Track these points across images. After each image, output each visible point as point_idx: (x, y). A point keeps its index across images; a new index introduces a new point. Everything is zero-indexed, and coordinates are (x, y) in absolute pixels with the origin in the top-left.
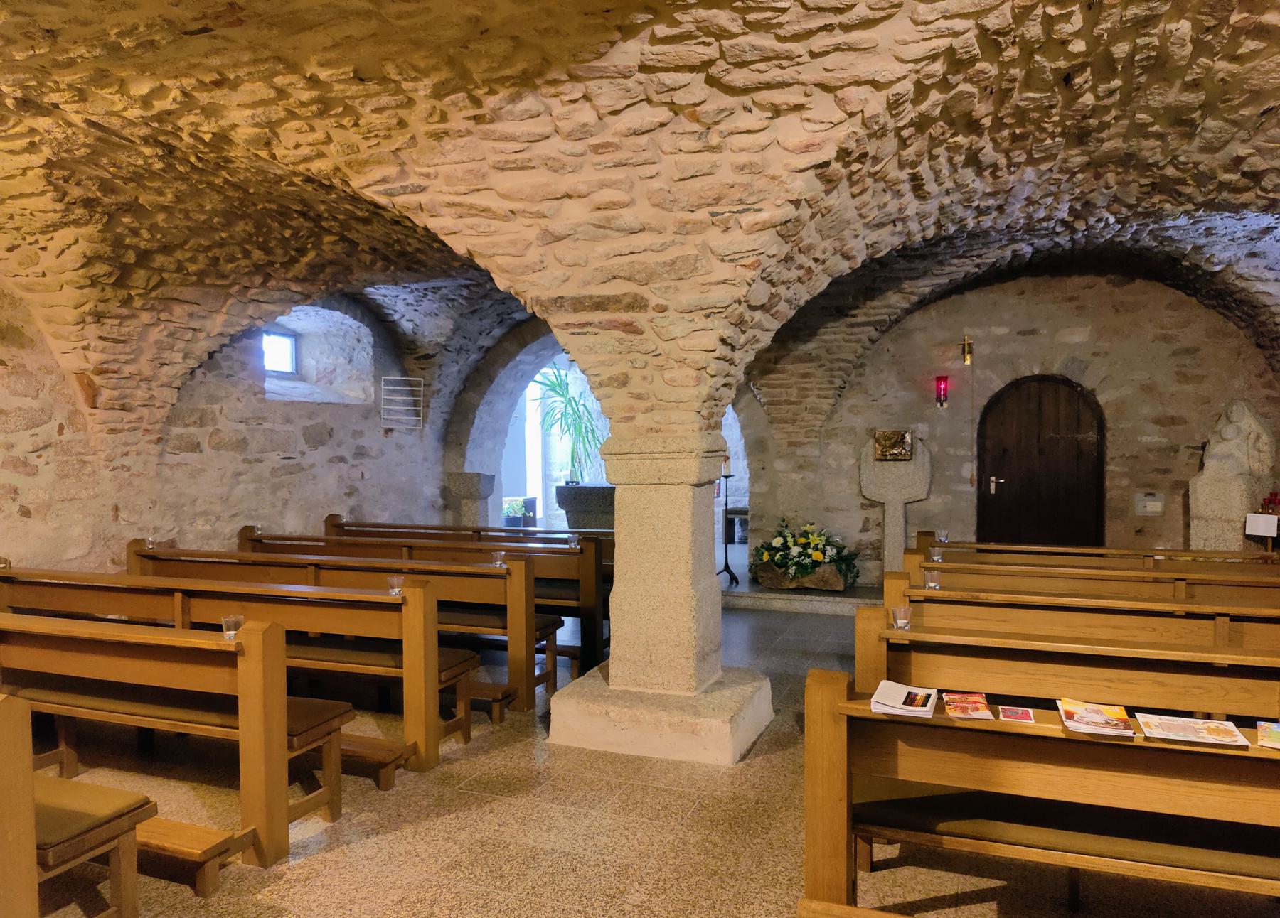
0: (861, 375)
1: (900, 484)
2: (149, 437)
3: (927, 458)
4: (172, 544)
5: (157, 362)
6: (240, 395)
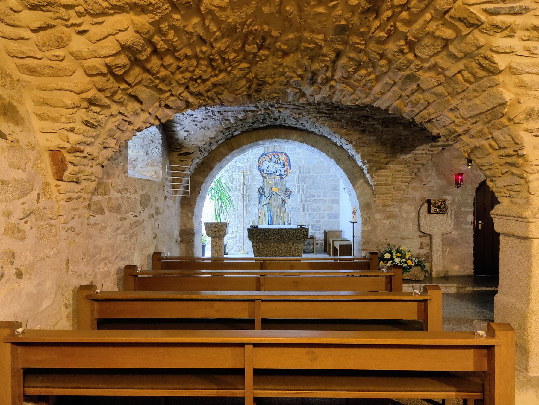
1: (439, 225)
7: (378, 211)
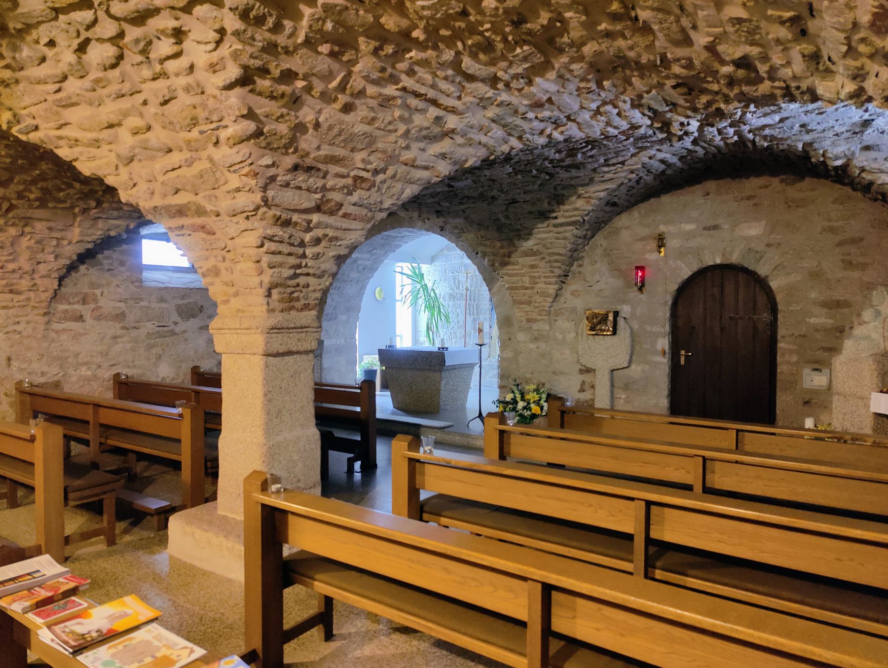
0: (581, 266)
1: (608, 352)
2: (35, 312)
3: (628, 334)
4: (57, 385)
5: (33, 261)
6: (119, 283)
7: (522, 329)
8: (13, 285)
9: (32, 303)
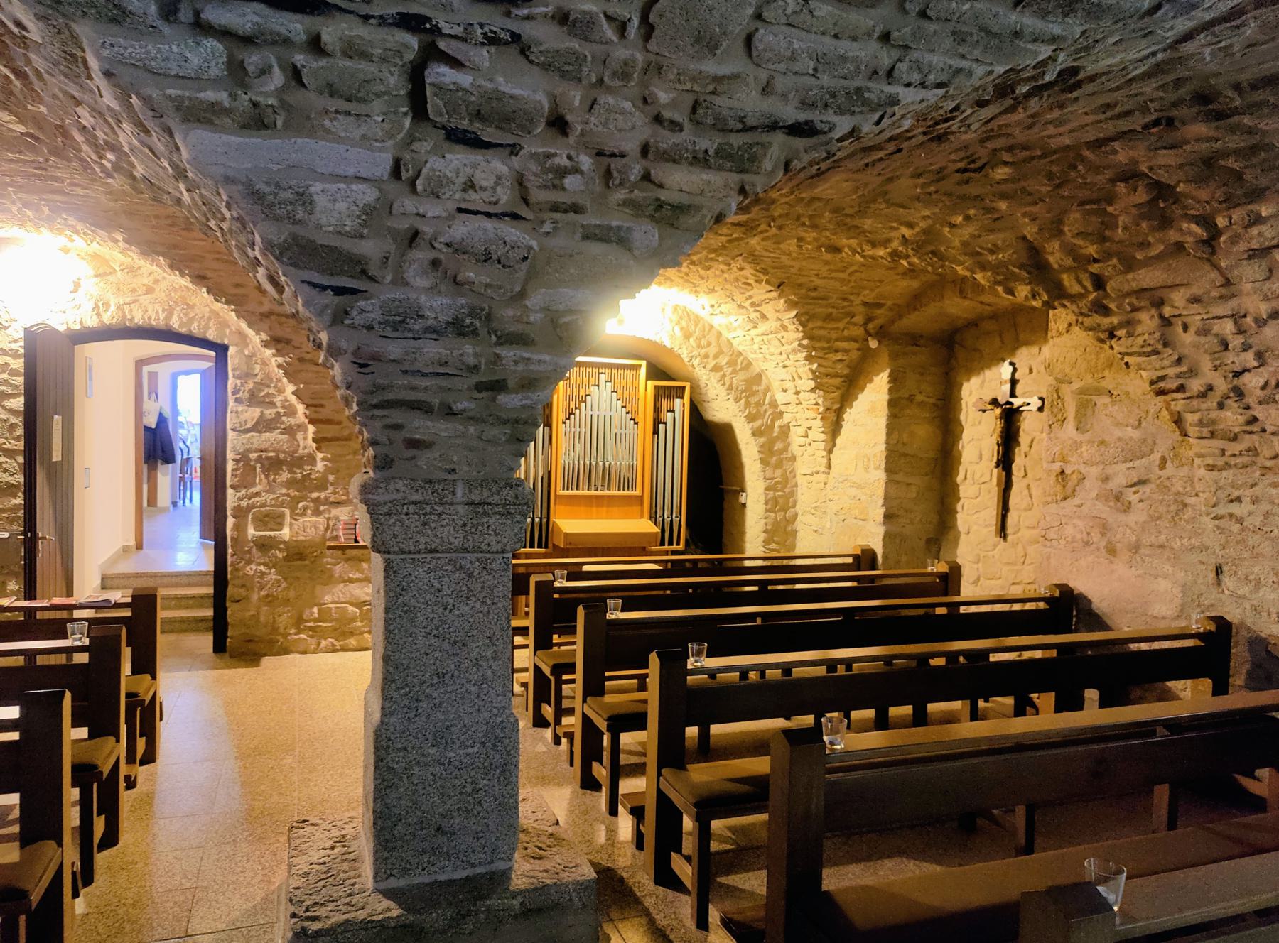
8: (1214, 422)
9: (1261, 460)
